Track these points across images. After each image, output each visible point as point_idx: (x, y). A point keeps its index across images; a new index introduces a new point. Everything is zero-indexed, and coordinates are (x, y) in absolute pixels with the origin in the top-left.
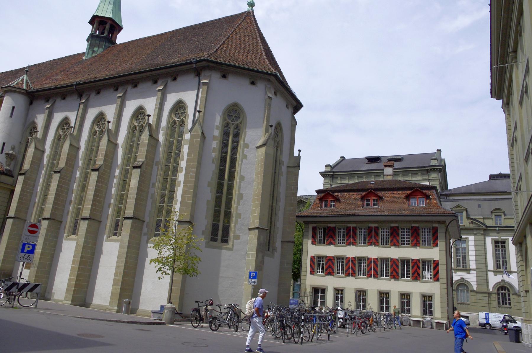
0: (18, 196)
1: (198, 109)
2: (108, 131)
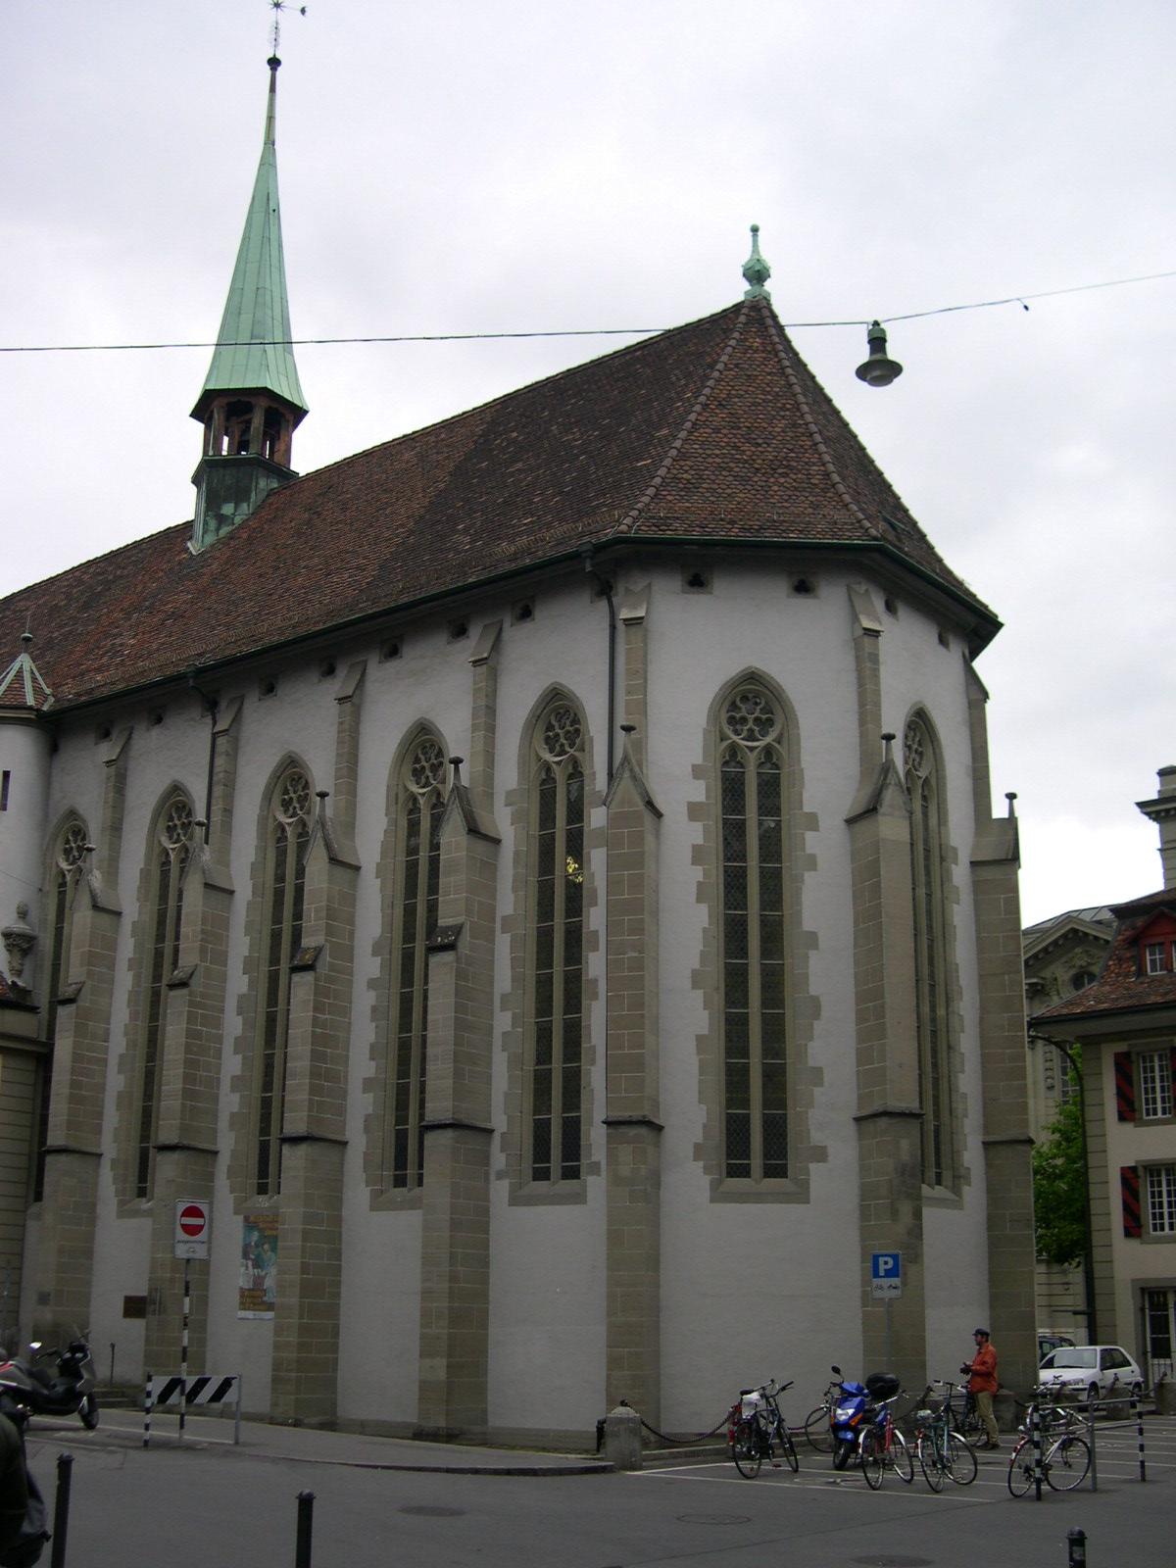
1: (621, 719)
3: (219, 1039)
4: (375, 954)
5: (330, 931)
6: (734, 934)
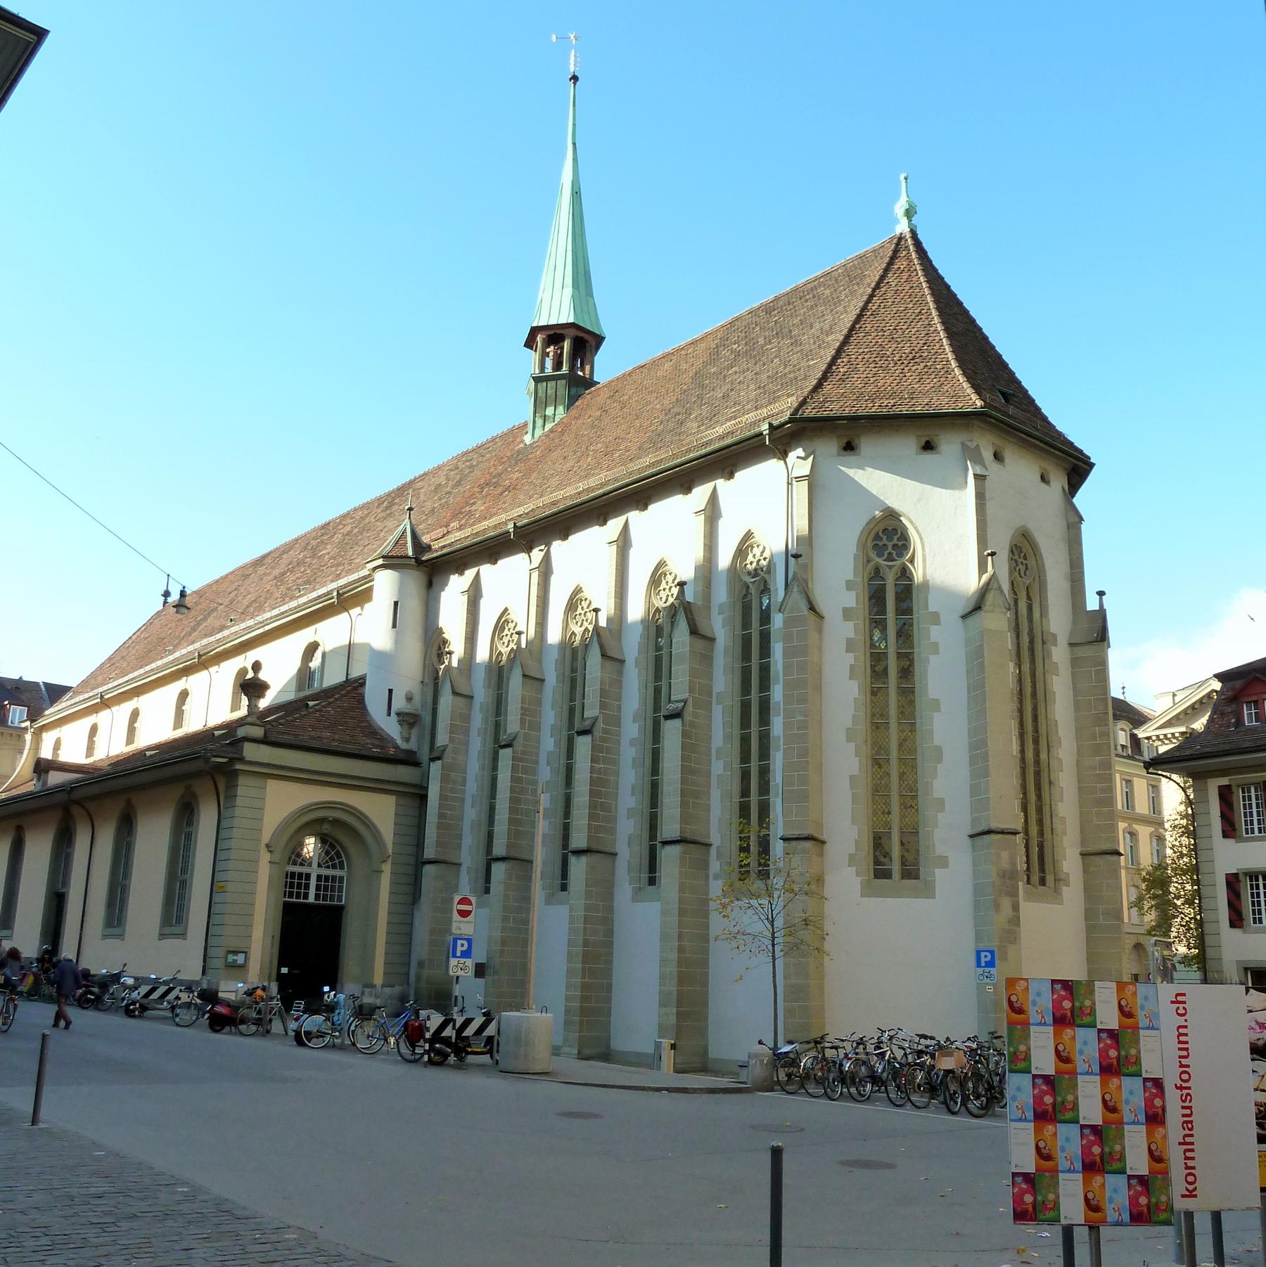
4: (634, 721)
5: (603, 706)
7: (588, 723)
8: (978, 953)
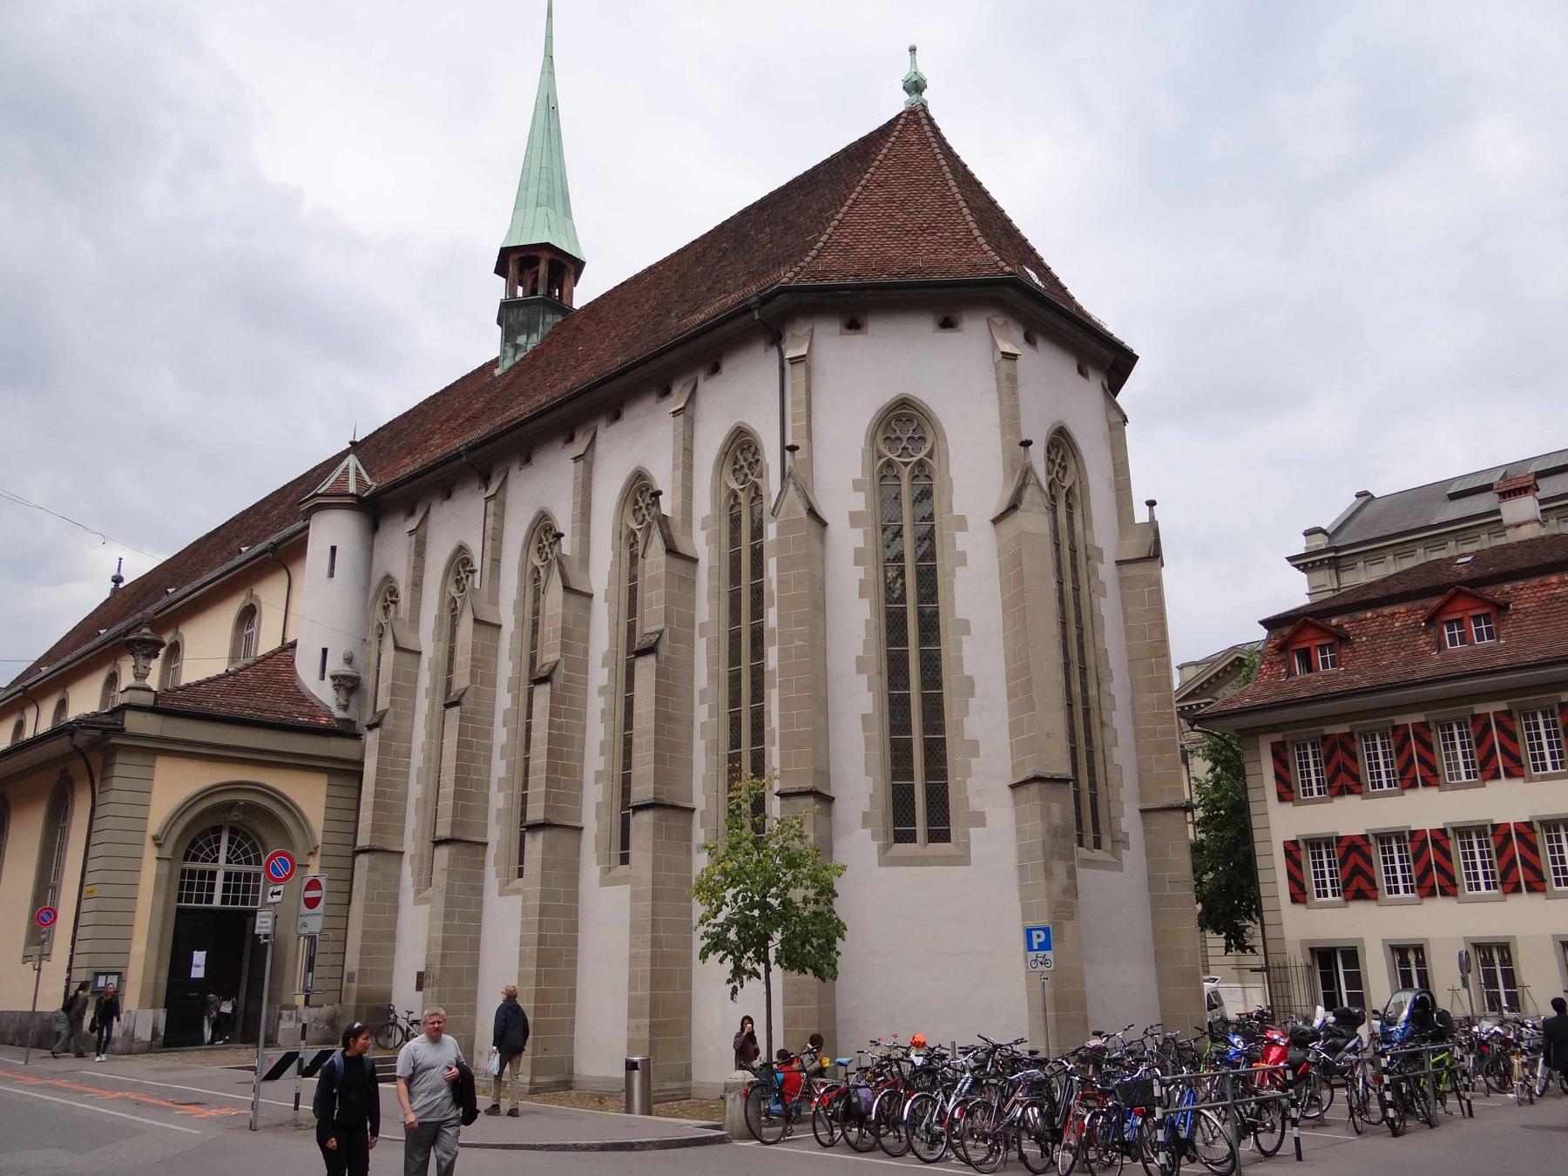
0: (372, 788)
2: (560, 563)
3: (490, 748)
5: (565, 648)
6: (894, 624)
7: (546, 668)
8: (1029, 932)
